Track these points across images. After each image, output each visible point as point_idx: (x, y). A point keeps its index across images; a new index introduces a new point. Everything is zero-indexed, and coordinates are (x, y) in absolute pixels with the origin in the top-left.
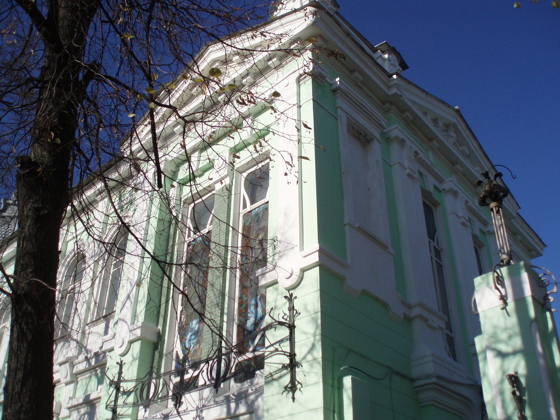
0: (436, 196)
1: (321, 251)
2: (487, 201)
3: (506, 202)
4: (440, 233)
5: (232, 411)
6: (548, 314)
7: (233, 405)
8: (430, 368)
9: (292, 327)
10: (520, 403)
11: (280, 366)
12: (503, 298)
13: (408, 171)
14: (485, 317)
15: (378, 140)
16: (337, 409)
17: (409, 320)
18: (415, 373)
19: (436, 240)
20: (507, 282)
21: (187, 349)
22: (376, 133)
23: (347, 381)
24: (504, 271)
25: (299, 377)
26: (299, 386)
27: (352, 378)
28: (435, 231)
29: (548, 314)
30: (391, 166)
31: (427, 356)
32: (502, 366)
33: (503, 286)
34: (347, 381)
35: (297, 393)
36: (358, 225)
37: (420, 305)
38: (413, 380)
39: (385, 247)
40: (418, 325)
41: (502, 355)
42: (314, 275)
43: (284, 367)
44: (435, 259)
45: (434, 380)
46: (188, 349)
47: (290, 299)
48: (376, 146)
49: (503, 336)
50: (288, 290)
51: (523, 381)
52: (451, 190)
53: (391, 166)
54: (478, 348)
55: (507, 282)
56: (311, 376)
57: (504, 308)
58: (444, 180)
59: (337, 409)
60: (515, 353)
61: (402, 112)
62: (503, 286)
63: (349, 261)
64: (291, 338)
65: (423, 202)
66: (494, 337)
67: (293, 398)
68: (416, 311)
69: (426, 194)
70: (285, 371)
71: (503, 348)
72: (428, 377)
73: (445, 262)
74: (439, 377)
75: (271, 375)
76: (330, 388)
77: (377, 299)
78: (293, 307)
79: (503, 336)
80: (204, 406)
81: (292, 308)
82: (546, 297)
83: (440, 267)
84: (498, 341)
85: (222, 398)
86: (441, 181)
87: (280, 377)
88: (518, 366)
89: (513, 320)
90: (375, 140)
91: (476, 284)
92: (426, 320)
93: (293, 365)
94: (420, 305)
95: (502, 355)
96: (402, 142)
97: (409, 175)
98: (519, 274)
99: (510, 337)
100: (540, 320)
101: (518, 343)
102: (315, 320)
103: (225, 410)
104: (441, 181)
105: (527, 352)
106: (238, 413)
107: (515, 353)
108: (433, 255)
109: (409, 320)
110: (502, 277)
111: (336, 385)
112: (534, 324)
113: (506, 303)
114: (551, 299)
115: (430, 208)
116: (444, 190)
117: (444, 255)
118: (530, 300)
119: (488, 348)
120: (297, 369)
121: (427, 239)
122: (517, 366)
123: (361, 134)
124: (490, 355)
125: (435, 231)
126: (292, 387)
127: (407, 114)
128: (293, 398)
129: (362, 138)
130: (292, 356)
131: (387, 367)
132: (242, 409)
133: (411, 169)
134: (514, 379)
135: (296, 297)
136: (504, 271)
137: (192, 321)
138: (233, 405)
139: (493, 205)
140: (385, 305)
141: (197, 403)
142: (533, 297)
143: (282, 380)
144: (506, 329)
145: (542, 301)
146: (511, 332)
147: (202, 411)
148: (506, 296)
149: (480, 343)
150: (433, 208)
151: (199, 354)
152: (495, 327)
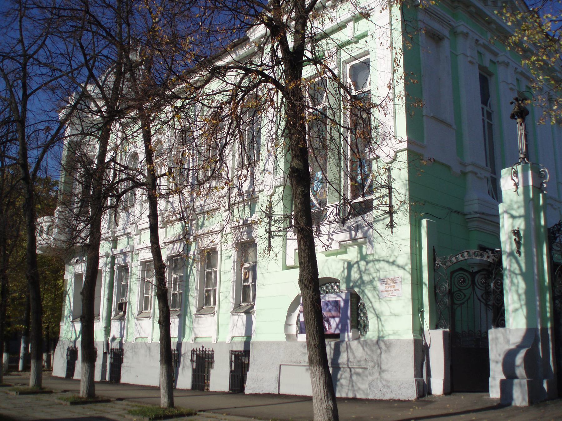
0: (491, 69)
1: (409, 142)
2: (516, 117)
3: (528, 118)
4: (492, 100)
5: (353, 236)
6: (541, 195)
7: (353, 233)
8: (476, 207)
9: (390, 188)
10: (518, 243)
11: (383, 212)
12: (516, 185)
13: (469, 59)
14: (506, 194)
15: (447, 38)
16: (417, 239)
17: (464, 174)
18: (466, 210)
19: (488, 105)
20: (520, 175)
21: (315, 191)
22: (446, 32)
23: (424, 222)
24: (519, 168)
25: (396, 220)
26: (395, 225)
27: (427, 221)
28: (489, 96)
29: (541, 195)
30: (457, 55)
31: (474, 202)
32: (512, 223)
33: (517, 177)
34: (424, 222)
35: (394, 230)
36: (432, 115)
37: (473, 164)
38: (465, 215)
39: (449, 126)
40: (470, 177)
41: (513, 217)
42: (404, 156)
43: (386, 213)
44: (486, 120)
45: (478, 215)
46: (316, 192)
47: (389, 170)
48: (446, 44)
49: (515, 206)
50: (388, 163)
51: (522, 233)
52: (504, 63)
53: (457, 55)
54: (501, 211)
55: (520, 175)
56: (403, 219)
57: (516, 191)
58: (498, 54)
59: (417, 239)
60: (520, 217)
61: (468, 6)
62: (517, 177)
63: (425, 143)
64: (390, 195)
65: (480, 74)
66: (510, 207)
67: (392, 232)
68: (469, 169)
69: (482, 69)
70: (387, 215)
71: (514, 213)
72: (474, 213)
73: (495, 121)
74: (482, 213)
75: (379, 216)
76: (414, 227)
77: (443, 164)
78: (391, 176)
79: (515, 206)
80: (333, 232)
81: (390, 176)
82: (542, 184)
83: (490, 126)
84: (513, 209)
85: (345, 228)
86: (496, 54)
87: (384, 219)
88: (520, 224)
89: (521, 198)
90: (446, 39)
91: (502, 174)
92: (476, 174)
93: (391, 212)
94: (473, 164)
95: (513, 217)
96: (466, 35)
97: (470, 62)
98: (527, 171)
99: (519, 207)
100: (536, 199)
101: (522, 211)
102: (405, 185)
103: (348, 235)
104: (496, 54)
105: (526, 217)
106: (357, 238)
107: (520, 217)
108: (485, 118)
109: (464, 174)
110: (517, 171)
111: (417, 224)
112: (531, 203)
113: (517, 188)
114: (545, 185)
115: (485, 80)
116: (498, 62)
117: (494, 116)
118: (531, 187)
119: (506, 212)
120: (394, 215)
121: (481, 105)
122: (520, 225)
123: (434, 35)
124: (506, 216)
125: (489, 96)
126: (391, 226)
127: (472, 9)
128: (392, 232)
129: (436, 38)
130: (391, 206)
131: (449, 208)
132: (360, 235)
133: (472, 57)
134: (516, 233)
135: (392, 169)
136: (519, 168)
137: (316, 172)
138: (353, 233)
139: (519, 120)
140: (449, 168)
141: (329, 230)
142: (532, 186)
143: (385, 221)
144: (517, 202)
145: (539, 186)
146: (519, 204)
147: (332, 235)
148: (518, 183)
149: (501, 208)
150: (488, 77)
151: (324, 196)
152: (511, 201)
